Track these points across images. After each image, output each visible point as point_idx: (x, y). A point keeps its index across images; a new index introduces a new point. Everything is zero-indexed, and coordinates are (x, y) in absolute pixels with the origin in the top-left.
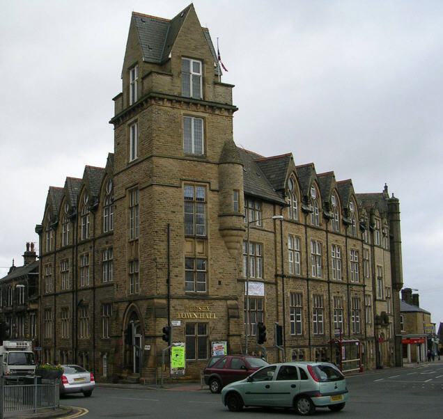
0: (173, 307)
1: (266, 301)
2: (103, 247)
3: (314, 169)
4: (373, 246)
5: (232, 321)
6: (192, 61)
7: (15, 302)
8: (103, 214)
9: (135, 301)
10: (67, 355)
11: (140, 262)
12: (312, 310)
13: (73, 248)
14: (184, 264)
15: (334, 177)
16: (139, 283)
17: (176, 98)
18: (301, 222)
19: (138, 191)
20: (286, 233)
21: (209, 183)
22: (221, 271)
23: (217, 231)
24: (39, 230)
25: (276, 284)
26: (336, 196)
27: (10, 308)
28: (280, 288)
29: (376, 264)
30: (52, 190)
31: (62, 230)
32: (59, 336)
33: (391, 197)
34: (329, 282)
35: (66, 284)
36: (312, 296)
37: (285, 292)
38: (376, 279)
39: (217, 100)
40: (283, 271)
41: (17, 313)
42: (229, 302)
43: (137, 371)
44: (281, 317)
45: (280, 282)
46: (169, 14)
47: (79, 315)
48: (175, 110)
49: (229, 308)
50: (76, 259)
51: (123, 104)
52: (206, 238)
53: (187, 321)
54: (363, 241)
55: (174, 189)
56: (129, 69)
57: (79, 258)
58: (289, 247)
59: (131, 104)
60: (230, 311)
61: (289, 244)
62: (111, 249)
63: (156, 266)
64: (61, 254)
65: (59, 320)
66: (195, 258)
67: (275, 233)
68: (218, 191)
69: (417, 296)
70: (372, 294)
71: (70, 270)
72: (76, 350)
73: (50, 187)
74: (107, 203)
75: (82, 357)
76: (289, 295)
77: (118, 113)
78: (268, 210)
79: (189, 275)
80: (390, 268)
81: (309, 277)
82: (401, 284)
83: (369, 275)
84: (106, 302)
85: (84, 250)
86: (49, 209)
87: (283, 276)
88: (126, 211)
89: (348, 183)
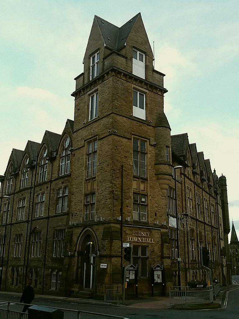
10: (18, 271)
21: (149, 139)
22: (157, 205)
23: (154, 175)
30: (15, 152)
32: (12, 256)
42: (163, 230)
47: (32, 239)
49: (162, 235)
52: (146, 180)
53: (134, 244)
55: (126, 140)
56: (91, 55)
59: (91, 80)
63: (113, 197)
64: (20, 194)
65: (12, 243)
66: (139, 194)
68: (154, 146)
75: (32, 273)
77: (78, 88)
84: (58, 228)
86: (12, 165)
88: (85, 157)
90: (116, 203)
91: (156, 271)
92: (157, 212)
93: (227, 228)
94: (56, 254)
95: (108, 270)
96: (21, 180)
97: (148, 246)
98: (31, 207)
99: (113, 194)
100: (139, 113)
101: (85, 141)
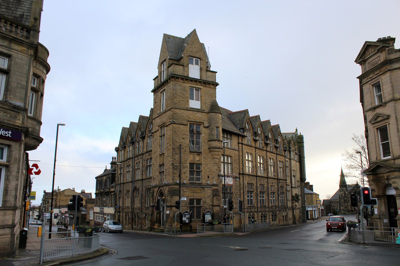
0: (182, 190)
1: (234, 187)
2: (147, 158)
3: (259, 118)
4: (290, 159)
5: (215, 198)
6: (194, 59)
7: (105, 187)
8: (147, 140)
9: (162, 186)
10: (128, 216)
11: (165, 165)
12: (259, 192)
13: (133, 159)
14: (189, 167)
15: (270, 123)
16: (164, 177)
17: (186, 78)
18: (253, 146)
19: (165, 127)
20: (245, 151)
21: (203, 123)
22: (209, 170)
24: (117, 150)
25: (239, 178)
26: (271, 133)
27: (102, 191)
28: (241, 180)
29: (292, 169)
31: (128, 149)
33: (299, 134)
34: (268, 178)
35: (129, 178)
36: (259, 185)
37: (244, 182)
38: (292, 176)
39: (208, 80)
40: (243, 171)
41: (105, 193)
42: (214, 188)
43: (163, 225)
44: (242, 196)
45: (241, 177)
46: (183, 35)
47: (135, 194)
48: (185, 84)
49: (214, 190)
50: (134, 165)
51: (158, 82)
52: (201, 153)
54: (285, 156)
57: (135, 164)
58: (247, 159)
59: (162, 81)
60: (214, 192)
61: (247, 157)
62: (151, 159)
64: (127, 162)
65: (125, 197)
67: (239, 151)
69: (312, 186)
70: (290, 185)
71: (131, 170)
72: (133, 213)
73: (123, 127)
74: (150, 135)
75: (135, 217)
76: (246, 184)
78: (235, 140)
79: (192, 173)
80: (299, 171)
81: (257, 175)
82: (305, 179)
83: (288, 174)
84: (148, 187)
85: (138, 160)
87: (243, 174)
88: (159, 138)
89: (277, 127)
90: (175, 171)
91: (207, 215)
92: (209, 175)
93: (303, 178)
94: (147, 205)
95: (170, 215)
96: (127, 152)
97: (201, 199)
98: (133, 171)
99: (173, 165)
100: (195, 104)
101: (159, 126)
